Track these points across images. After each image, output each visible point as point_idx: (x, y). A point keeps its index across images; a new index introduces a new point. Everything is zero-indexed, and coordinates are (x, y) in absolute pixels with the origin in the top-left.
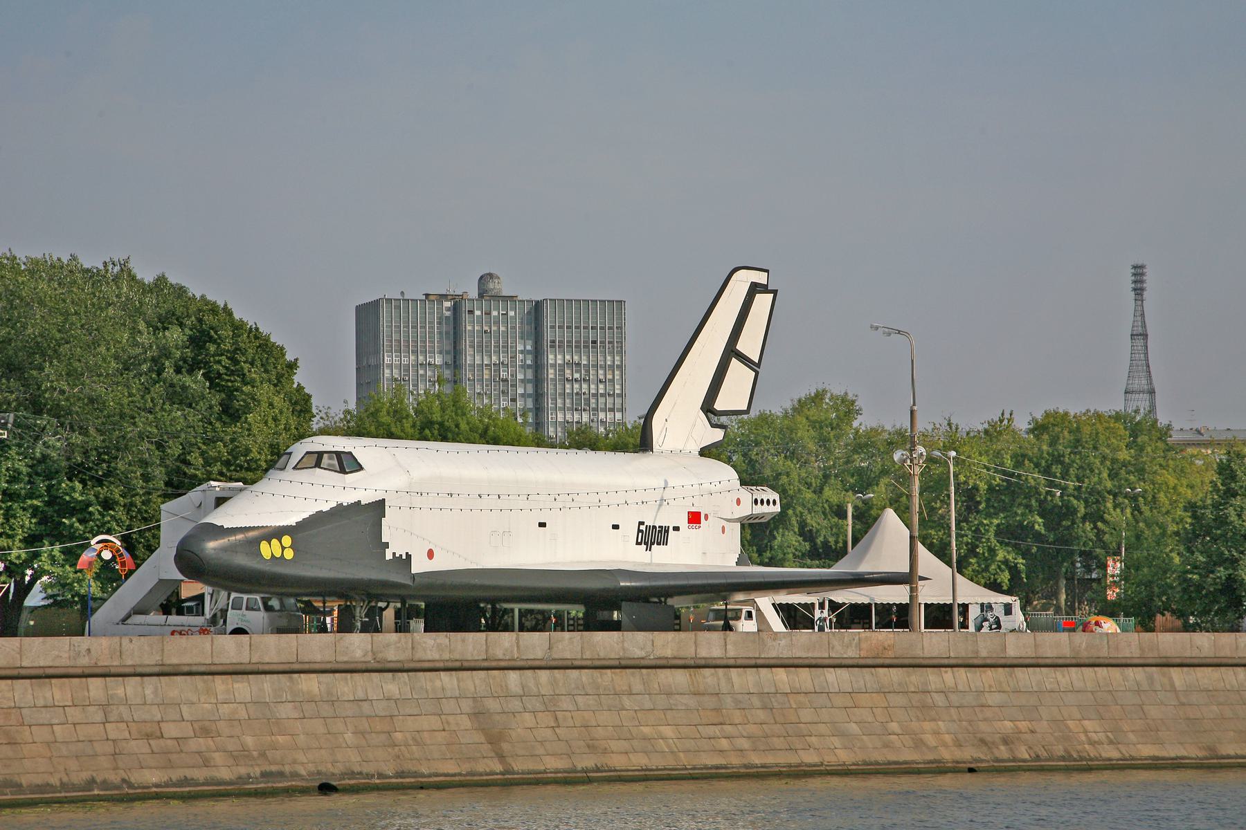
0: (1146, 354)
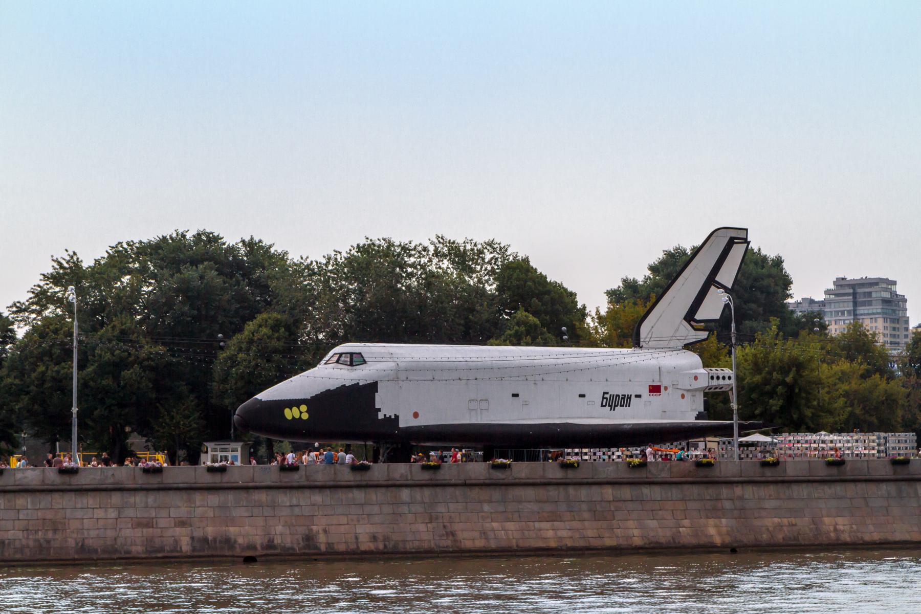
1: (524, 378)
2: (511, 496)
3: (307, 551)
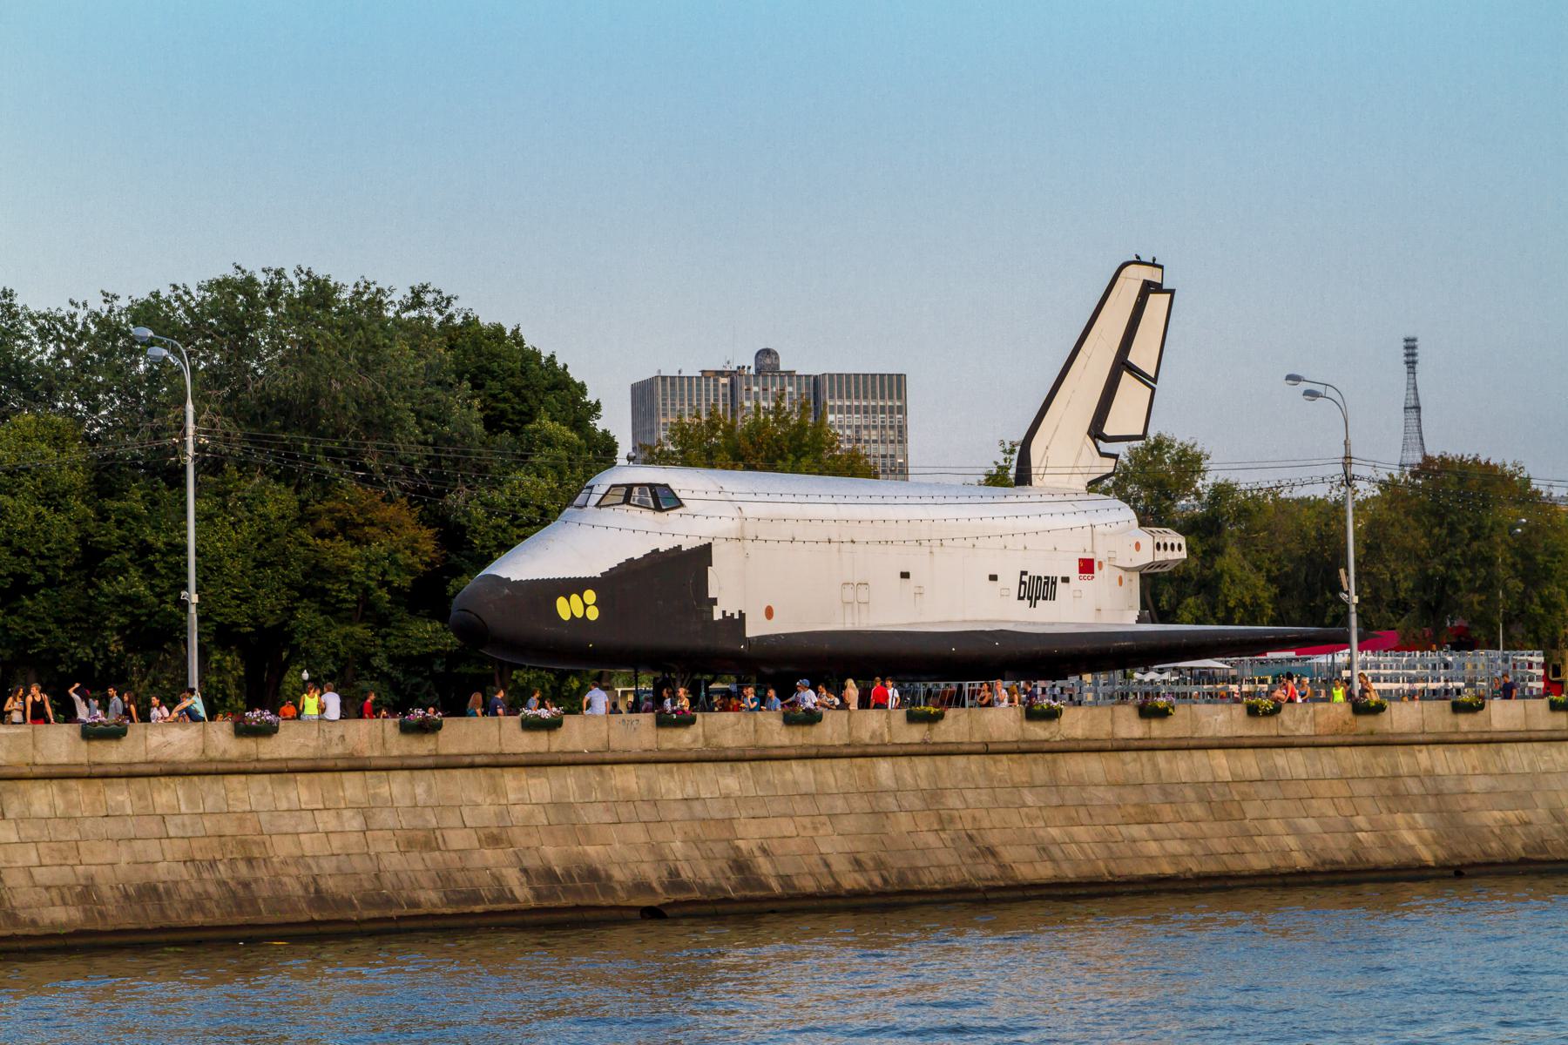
0: (1419, 426)
1: (969, 543)
3: (748, 893)
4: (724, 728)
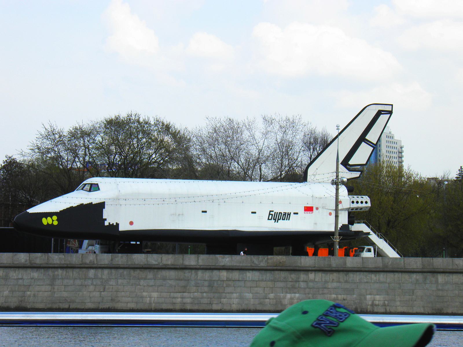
2: (159, 276)
4: (36, 258)
